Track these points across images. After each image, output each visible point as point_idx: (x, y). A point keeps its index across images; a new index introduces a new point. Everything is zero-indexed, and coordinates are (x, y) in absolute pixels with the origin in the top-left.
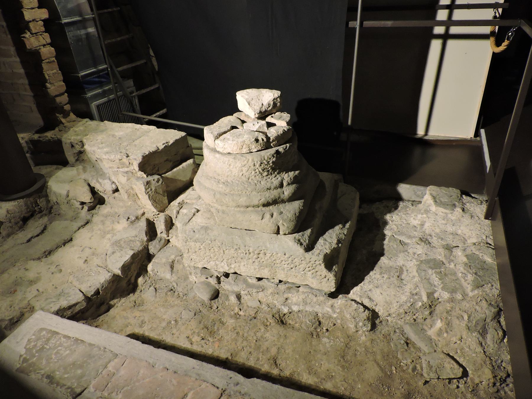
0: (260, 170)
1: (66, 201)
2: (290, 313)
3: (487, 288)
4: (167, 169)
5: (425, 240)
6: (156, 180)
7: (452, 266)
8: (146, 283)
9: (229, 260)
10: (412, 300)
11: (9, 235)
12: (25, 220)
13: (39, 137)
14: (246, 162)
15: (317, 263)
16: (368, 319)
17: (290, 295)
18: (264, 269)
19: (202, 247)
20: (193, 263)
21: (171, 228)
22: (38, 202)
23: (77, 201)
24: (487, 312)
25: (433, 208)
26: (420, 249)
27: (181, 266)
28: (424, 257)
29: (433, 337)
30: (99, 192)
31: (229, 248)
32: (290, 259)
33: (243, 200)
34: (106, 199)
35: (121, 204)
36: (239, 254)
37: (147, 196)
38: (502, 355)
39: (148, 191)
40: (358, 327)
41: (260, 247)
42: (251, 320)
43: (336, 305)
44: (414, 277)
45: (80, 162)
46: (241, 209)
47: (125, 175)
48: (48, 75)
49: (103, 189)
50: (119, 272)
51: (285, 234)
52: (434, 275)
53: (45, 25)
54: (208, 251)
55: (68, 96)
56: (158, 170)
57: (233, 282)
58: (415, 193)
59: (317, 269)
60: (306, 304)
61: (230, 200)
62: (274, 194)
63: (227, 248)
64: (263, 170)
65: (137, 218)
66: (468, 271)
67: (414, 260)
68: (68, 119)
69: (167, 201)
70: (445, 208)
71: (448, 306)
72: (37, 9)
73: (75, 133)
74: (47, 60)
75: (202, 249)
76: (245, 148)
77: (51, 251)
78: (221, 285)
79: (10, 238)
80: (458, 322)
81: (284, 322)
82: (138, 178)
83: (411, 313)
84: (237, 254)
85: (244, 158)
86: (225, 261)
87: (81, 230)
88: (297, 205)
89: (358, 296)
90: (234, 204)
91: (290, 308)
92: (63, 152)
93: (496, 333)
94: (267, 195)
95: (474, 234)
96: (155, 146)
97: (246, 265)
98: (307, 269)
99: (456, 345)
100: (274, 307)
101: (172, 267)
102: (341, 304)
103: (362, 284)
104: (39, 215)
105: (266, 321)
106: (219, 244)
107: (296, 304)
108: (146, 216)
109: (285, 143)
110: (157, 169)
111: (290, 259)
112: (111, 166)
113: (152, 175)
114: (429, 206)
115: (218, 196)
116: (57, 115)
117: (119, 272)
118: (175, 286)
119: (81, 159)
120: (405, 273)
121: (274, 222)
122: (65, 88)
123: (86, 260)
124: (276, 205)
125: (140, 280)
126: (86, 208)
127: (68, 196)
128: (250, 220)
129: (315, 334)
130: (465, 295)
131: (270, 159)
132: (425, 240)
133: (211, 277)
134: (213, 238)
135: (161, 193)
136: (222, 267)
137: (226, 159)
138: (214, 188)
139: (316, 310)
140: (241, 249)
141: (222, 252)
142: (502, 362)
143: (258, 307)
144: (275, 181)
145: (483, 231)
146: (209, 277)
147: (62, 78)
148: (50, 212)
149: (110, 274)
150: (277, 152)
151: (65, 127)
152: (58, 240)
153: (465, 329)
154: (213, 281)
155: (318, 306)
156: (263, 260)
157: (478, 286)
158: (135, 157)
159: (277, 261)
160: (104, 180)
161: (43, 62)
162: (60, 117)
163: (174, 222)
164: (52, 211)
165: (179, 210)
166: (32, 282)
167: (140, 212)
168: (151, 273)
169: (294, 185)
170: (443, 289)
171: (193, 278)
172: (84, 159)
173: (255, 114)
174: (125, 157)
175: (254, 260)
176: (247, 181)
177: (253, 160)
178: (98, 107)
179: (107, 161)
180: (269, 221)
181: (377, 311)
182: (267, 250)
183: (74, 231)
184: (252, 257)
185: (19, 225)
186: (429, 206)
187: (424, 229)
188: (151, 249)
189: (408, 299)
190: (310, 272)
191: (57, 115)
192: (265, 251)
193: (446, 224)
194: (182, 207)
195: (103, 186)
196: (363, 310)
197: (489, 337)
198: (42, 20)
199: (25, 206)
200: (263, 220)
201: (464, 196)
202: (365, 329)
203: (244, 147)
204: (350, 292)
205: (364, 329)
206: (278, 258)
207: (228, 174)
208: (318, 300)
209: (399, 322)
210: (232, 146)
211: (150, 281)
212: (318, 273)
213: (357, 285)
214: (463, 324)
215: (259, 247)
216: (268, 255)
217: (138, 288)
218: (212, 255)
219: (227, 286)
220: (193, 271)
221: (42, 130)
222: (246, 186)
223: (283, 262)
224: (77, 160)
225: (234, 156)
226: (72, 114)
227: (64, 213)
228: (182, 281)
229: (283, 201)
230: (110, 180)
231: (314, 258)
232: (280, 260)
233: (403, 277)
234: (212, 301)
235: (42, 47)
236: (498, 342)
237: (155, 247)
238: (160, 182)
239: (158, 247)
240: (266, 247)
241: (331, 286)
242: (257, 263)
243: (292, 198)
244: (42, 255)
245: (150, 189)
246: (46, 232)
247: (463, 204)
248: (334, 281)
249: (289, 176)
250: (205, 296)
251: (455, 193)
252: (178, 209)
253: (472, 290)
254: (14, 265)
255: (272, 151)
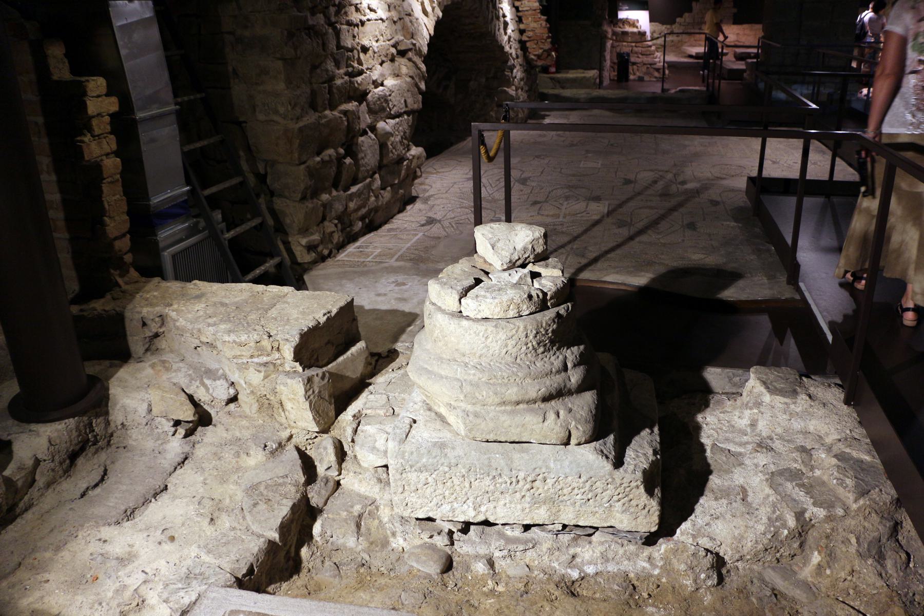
0: (534, 343)
1: (144, 421)
2: (583, 578)
3: (874, 494)
4: (329, 359)
5: (763, 446)
6: (320, 375)
7: (818, 473)
8: (314, 556)
9: (478, 499)
10: (772, 529)
11: (48, 485)
12: (73, 457)
13: (81, 310)
14: (514, 331)
15: (633, 484)
16: (712, 567)
17: (578, 550)
18: (538, 508)
19: (430, 479)
20: (410, 510)
21: (343, 460)
22: (94, 425)
23: (168, 420)
24: (880, 528)
25: (767, 398)
26: (762, 459)
27: (376, 522)
28: (773, 468)
29: (810, 579)
30: (202, 404)
31: (482, 476)
32: (588, 485)
33: (512, 393)
34: (213, 415)
35: (244, 423)
36: (498, 485)
37: (307, 403)
38: (911, 585)
39: (308, 394)
40: (698, 581)
41: (537, 470)
42: (522, 596)
43: (656, 555)
44: (768, 496)
45: (153, 354)
46: (507, 408)
47: (262, 369)
48: (108, 202)
49: (210, 397)
50: (275, 536)
51: (579, 444)
52: (797, 488)
53: (111, 123)
54: (440, 486)
55: (131, 240)
56: (317, 360)
57: (478, 540)
58: (730, 380)
59: (631, 496)
60: (607, 560)
61: (491, 393)
62: (556, 381)
63: (478, 476)
64: (538, 344)
65: (281, 446)
66: (845, 475)
67: (760, 474)
68: (126, 279)
69: (333, 412)
70: (784, 396)
71: (827, 527)
72: (104, 97)
73: (146, 302)
74: (109, 180)
75: (430, 484)
76: (512, 310)
77: (136, 508)
78: (456, 546)
79: (50, 490)
80: (844, 549)
81: (576, 593)
82: (292, 374)
83: (773, 549)
84: (495, 485)
85: (512, 326)
86: (470, 503)
87: (178, 472)
88: (589, 397)
89: (689, 536)
90: (497, 400)
91: (581, 571)
92: (124, 336)
93: (898, 557)
94: (548, 383)
95: (833, 430)
96: (311, 317)
97: (507, 505)
98: (616, 498)
99: (846, 583)
100: (553, 572)
101: (358, 526)
102: (666, 551)
103: (693, 517)
104: (93, 449)
105: (548, 594)
106: (463, 470)
107: (590, 563)
108: (294, 440)
109: (566, 302)
110: (315, 357)
111: (588, 485)
112: (239, 353)
113: (309, 367)
114: (759, 395)
115: (468, 388)
116: (112, 271)
117: (275, 536)
118: (367, 558)
119: (153, 347)
120: (750, 494)
121: (564, 424)
122: (128, 225)
123: (212, 519)
124: (561, 400)
125: (304, 552)
126: (181, 431)
127: (150, 411)
128: (524, 425)
129: (631, 602)
130: (846, 509)
131: (550, 325)
132: (763, 446)
133: (439, 534)
134: (453, 461)
135: (327, 398)
136: (464, 513)
137: (481, 328)
138: (458, 376)
139: (622, 568)
140: (503, 475)
141: (467, 485)
142: (914, 595)
143: (527, 576)
144: (555, 360)
145: (844, 423)
146: (436, 534)
147: (125, 208)
148: (109, 444)
149: (262, 540)
150: (558, 315)
151: (122, 292)
152: (141, 489)
153: (856, 556)
154: (441, 541)
155: (626, 562)
156: (540, 491)
157: (863, 493)
158: (287, 336)
159: (565, 491)
160: (215, 380)
161: (104, 181)
162: (115, 273)
163: (346, 450)
164: (112, 442)
165: (357, 428)
166: (122, 561)
167: (285, 435)
168: (318, 539)
169: (582, 367)
170: (815, 504)
171: (398, 543)
172: (159, 347)
173: (502, 264)
174: (266, 337)
175: (523, 494)
176: (513, 363)
177: (525, 327)
178: (174, 257)
179: (231, 345)
180: (556, 424)
181: (721, 554)
182: (549, 472)
183: (168, 472)
184: (521, 490)
185: (65, 466)
186: (759, 395)
187: (758, 431)
188: (313, 497)
189: (766, 528)
190: (620, 503)
191: (112, 271)
192: (546, 474)
193: (790, 420)
194: (359, 422)
195: (211, 391)
196: (704, 554)
197: (889, 564)
198: (109, 115)
199: (76, 431)
200: (546, 424)
201: (803, 378)
202: (709, 583)
203: (511, 307)
204: (676, 532)
205: (709, 584)
206: (568, 485)
207: (482, 352)
208: (625, 551)
209: (755, 567)
210: (493, 307)
211: (318, 553)
212: (634, 503)
213: (685, 519)
214: (853, 549)
215: (535, 469)
216: (550, 482)
217: (303, 565)
218: (447, 493)
219: (465, 547)
220: (399, 528)
221: (82, 298)
222: (515, 370)
223: (576, 491)
224: (147, 350)
225: (495, 323)
226: (132, 270)
227: (134, 443)
228: (377, 549)
229: (570, 393)
230: (227, 380)
231: (628, 477)
232: (570, 488)
233: (749, 499)
234: (445, 575)
235: (104, 158)
236: (903, 568)
237: (319, 493)
238: (326, 380)
239: (325, 494)
240: (547, 467)
241: (649, 522)
242: (528, 499)
243: (582, 388)
244: (122, 517)
245: (311, 390)
246: (105, 485)
247: (807, 389)
248: (657, 513)
249: (573, 353)
250: (433, 569)
251: (791, 374)
252: (355, 426)
253: (856, 501)
254: (75, 535)
255: (550, 314)
